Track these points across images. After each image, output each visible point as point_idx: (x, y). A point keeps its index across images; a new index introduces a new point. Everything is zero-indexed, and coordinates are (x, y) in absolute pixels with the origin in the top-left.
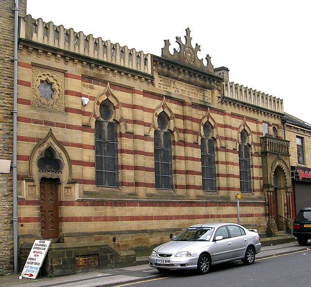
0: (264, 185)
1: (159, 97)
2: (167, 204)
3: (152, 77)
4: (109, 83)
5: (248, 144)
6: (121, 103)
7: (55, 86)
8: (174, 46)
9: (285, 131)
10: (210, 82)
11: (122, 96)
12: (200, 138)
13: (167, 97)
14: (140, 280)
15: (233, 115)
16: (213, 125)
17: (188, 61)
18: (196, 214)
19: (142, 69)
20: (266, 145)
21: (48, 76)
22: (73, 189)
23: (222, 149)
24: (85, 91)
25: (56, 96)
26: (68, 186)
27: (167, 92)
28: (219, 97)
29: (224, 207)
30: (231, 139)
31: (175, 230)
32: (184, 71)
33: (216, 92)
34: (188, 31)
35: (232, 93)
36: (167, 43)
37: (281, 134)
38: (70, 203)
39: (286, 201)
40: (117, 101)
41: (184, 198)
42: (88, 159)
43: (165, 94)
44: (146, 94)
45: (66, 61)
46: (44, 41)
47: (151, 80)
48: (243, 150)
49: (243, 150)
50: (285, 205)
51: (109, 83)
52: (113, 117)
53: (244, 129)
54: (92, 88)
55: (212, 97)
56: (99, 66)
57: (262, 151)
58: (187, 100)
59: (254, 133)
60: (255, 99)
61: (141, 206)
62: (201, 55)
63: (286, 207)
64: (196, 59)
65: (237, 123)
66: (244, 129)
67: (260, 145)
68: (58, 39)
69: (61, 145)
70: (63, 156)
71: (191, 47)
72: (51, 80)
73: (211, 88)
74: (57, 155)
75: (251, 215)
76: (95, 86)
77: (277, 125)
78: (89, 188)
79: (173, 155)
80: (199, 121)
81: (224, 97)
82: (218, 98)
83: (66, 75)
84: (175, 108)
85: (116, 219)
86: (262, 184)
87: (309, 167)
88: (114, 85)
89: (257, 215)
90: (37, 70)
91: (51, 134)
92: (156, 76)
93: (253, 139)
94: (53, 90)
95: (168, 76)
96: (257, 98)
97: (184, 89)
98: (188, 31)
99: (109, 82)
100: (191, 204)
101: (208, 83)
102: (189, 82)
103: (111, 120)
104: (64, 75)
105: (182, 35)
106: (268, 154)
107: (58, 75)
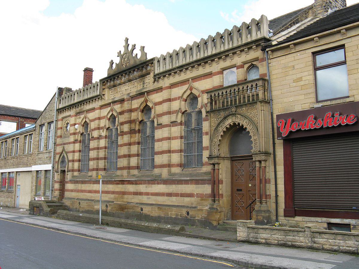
1: (181, 84)
2: (83, 182)
8: (117, 60)
10: (146, 68)
11: (91, 116)
15: (173, 86)
18: (126, 190)
23: (159, 126)
29: (153, 185)
31: (109, 202)
32: (122, 75)
35: (80, 97)
43: (111, 101)
55: (149, 83)
56: (252, 47)
58: (125, 97)
61: (93, 184)
62: (137, 52)
65: (178, 92)
68: (250, 33)
75: (190, 195)
78: (76, 174)
84: (118, 108)
85: (170, 195)
88: (195, 79)
89: (199, 195)
93: (204, 99)
95: (114, 86)
96: (65, 100)
99: (85, 110)
100: (122, 182)
101: (144, 71)
102: (130, 81)
103: (197, 110)
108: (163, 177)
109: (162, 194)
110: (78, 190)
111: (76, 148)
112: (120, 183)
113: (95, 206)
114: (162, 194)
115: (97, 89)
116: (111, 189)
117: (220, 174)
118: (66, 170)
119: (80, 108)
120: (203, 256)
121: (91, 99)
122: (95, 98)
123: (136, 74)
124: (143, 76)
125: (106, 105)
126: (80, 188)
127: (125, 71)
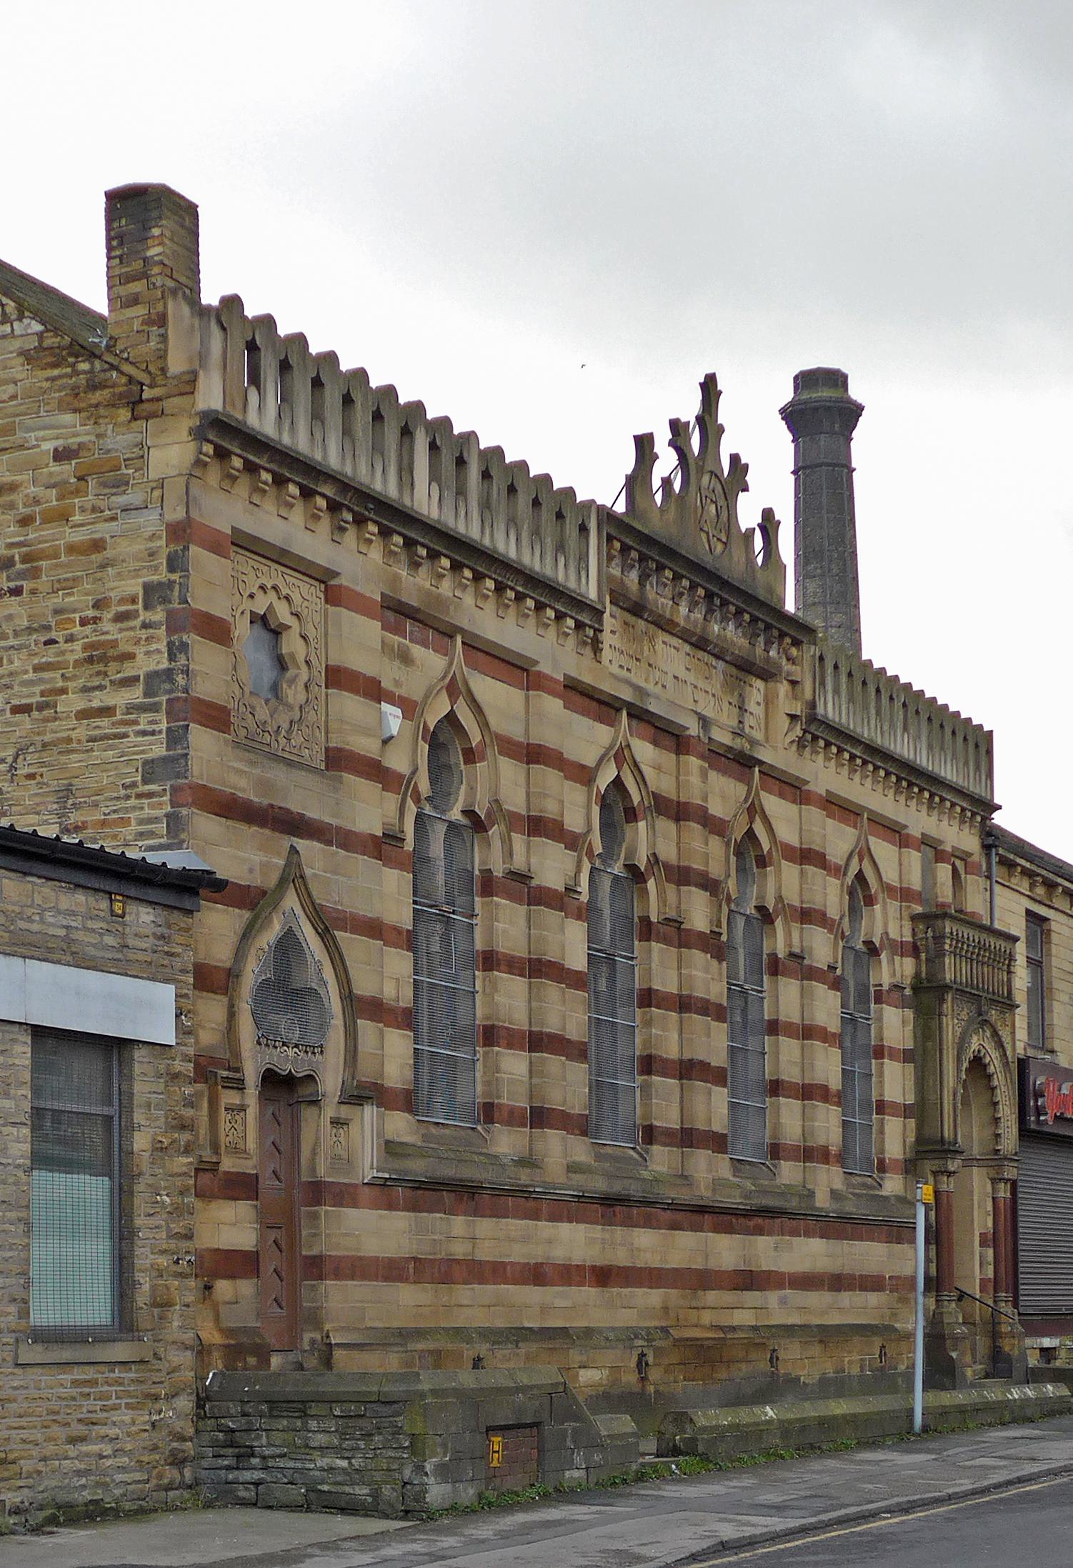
0: (920, 1140)
3: (598, 614)
4: (459, 639)
5: (468, 813)
6: (498, 737)
7: (292, 645)
9: (997, 888)
12: (411, 809)
13: (639, 715)
14: (803, 1530)
16: (475, 738)
17: (703, 547)
19: (563, 575)
20: (941, 954)
21: (272, 595)
22: (354, 1128)
24: (389, 674)
25: (295, 695)
26: (345, 1111)
27: (638, 689)
28: (793, 717)
30: (375, 771)
33: (783, 688)
34: (709, 388)
36: (644, 444)
37: (975, 903)
38: (345, 1196)
39: (990, 1224)
40: (484, 724)
41: (431, 1152)
42: (393, 994)
43: (626, 695)
44: (571, 694)
45: (391, 552)
46: (343, 463)
47: (595, 630)
48: (437, 848)
49: (437, 848)
50: (983, 1243)
51: (459, 639)
52: (461, 799)
53: (451, 718)
54: (405, 658)
57: (917, 975)
59: (889, 889)
60: (823, 683)
61: (554, 1218)
63: (990, 1252)
64: (733, 531)
66: (451, 718)
67: (910, 947)
69: (326, 923)
70: (328, 973)
71: (716, 474)
72: (283, 614)
73: (767, 675)
74: (312, 970)
76: (417, 651)
77: (964, 856)
79: (637, 986)
80: (584, 775)
81: (813, 718)
82: (787, 721)
83: (334, 595)
86: (911, 1138)
87: (1063, 1061)
90: (246, 563)
91: (293, 875)
92: (609, 607)
94: (281, 664)
97: (682, 673)
98: (709, 388)
104: (326, 592)
105: (689, 410)
106: (949, 997)
107: (305, 588)
108: (818, 1205)
109: (569, 1274)
110: (452, 1261)
111: (886, 1034)
112: (706, 1227)
113: (582, 1372)
114: (569, 1274)
115: (583, 558)
116: (648, 1255)
117: (991, 1213)
118: (331, 1081)
119: (423, 579)
120: (1020, 1480)
121: (853, 746)
122: (412, 535)
123: (729, 633)
124: (745, 668)
125: (591, 698)
126: (459, 1250)
127: (725, 584)
